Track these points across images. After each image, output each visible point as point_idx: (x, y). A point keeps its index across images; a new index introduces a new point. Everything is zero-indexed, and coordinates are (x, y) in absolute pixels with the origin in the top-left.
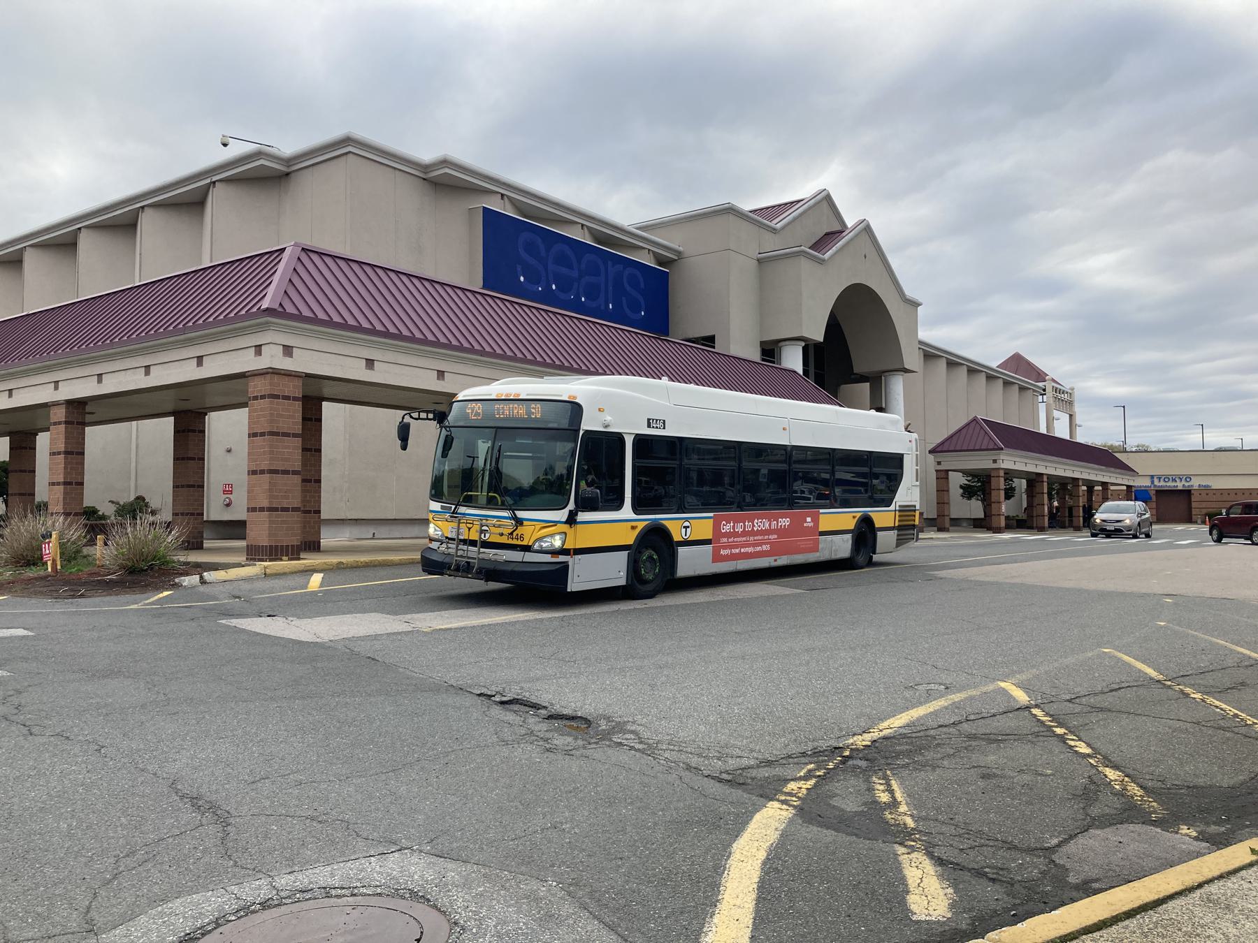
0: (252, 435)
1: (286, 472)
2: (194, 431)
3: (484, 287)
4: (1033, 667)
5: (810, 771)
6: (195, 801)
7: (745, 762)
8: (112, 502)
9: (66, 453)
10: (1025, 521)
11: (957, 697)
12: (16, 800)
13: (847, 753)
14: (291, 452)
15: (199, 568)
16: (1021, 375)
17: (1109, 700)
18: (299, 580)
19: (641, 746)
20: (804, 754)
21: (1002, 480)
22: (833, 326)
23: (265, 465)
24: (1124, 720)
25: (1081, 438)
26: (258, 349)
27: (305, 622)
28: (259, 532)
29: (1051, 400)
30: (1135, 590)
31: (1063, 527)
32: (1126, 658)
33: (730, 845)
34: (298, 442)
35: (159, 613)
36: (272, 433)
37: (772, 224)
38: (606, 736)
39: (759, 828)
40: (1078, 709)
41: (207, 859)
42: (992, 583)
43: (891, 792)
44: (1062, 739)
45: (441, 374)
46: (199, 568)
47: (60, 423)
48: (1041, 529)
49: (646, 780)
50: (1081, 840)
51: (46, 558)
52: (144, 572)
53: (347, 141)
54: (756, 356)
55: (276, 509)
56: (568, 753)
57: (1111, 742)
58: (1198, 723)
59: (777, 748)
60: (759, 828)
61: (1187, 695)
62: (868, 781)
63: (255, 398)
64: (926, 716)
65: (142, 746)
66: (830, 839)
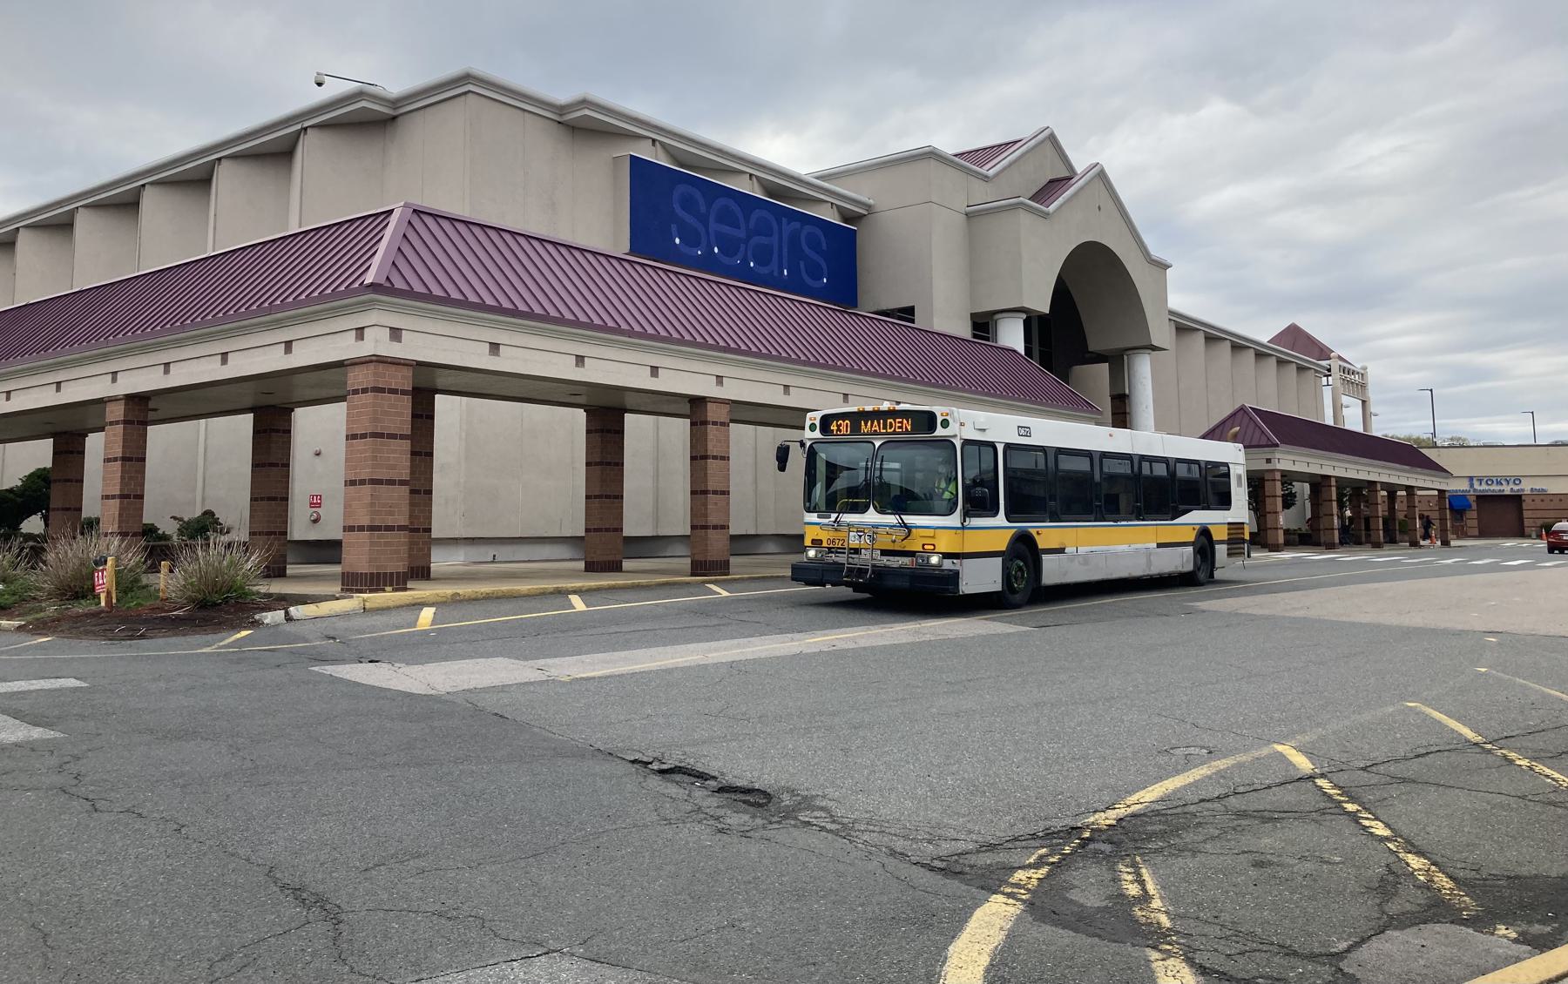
0: (351, 437)
1: (391, 482)
2: (278, 431)
3: (632, 252)
4: (1318, 725)
5: (1041, 857)
6: (297, 892)
7: (961, 846)
8: (174, 518)
9: (124, 459)
10: (1309, 536)
11: (1222, 764)
12: (85, 891)
13: (1087, 835)
14: (398, 457)
15: (285, 601)
16: (1299, 351)
17: (1413, 768)
18: (406, 616)
19: (833, 827)
20: (1034, 836)
21: (1279, 484)
22: (1061, 293)
23: (365, 474)
24: (1433, 794)
25: (1378, 430)
26: (360, 332)
27: (415, 670)
28: (358, 556)
29: (1338, 383)
30: (1449, 625)
31: (1358, 543)
32: (1437, 715)
33: (946, 948)
34: (406, 445)
35: (238, 658)
36: (375, 435)
37: (983, 171)
38: (789, 814)
39: (980, 927)
40: (1375, 779)
41: (317, 964)
42: (1267, 618)
43: (1142, 883)
44: (1354, 817)
45: (580, 360)
46: (285, 601)
47: (117, 423)
48: (1330, 546)
49: (841, 867)
50: (1375, 943)
51: (98, 589)
52: (219, 607)
53: (467, 78)
54: (964, 330)
55: (378, 528)
56: (745, 834)
57: (1416, 822)
58: (1523, 797)
59: (1000, 829)
60: (980, 927)
61: (1511, 762)
62: (1112, 869)
63: (356, 392)
64: (1185, 787)
65: (229, 825)
66: (1067, 941)
